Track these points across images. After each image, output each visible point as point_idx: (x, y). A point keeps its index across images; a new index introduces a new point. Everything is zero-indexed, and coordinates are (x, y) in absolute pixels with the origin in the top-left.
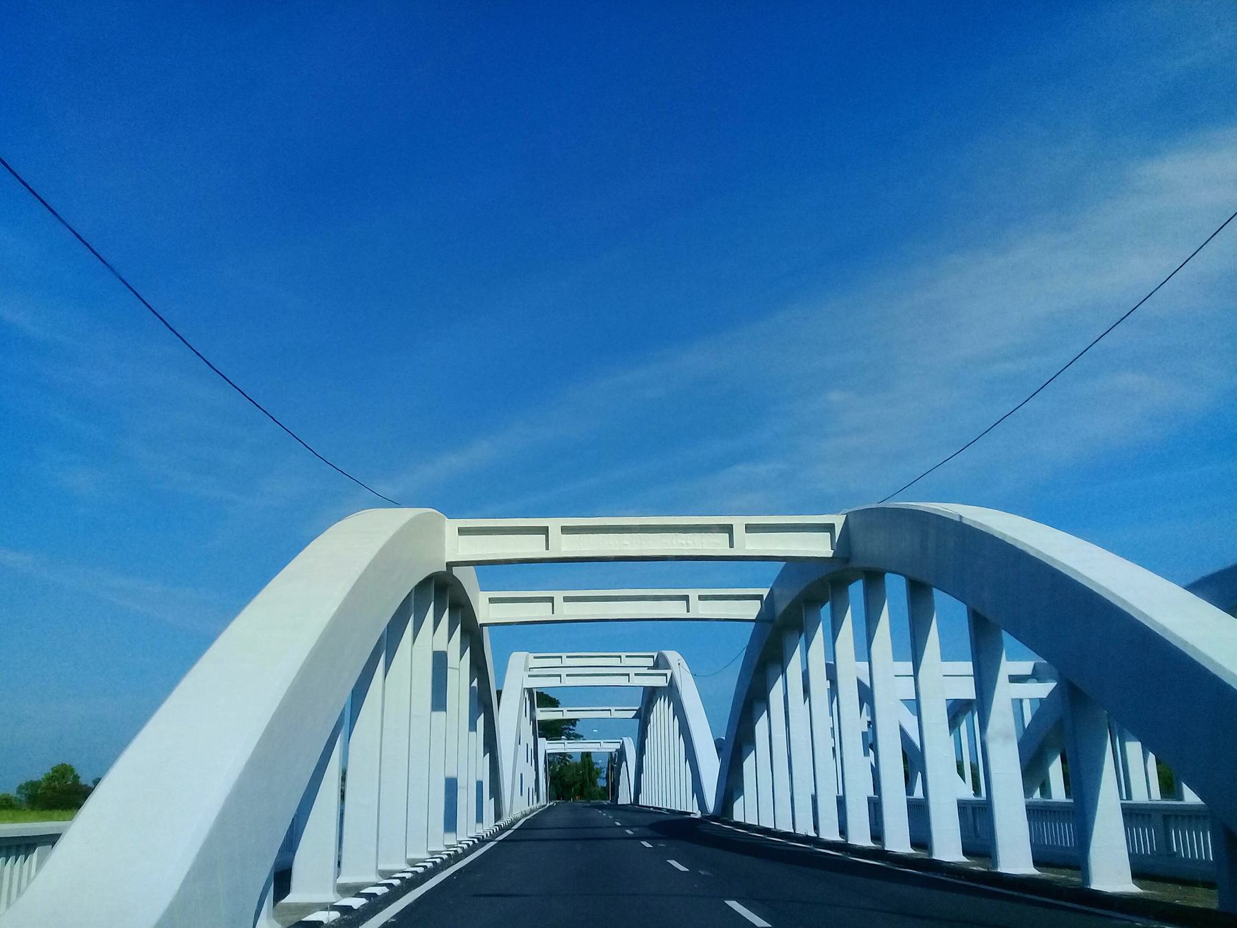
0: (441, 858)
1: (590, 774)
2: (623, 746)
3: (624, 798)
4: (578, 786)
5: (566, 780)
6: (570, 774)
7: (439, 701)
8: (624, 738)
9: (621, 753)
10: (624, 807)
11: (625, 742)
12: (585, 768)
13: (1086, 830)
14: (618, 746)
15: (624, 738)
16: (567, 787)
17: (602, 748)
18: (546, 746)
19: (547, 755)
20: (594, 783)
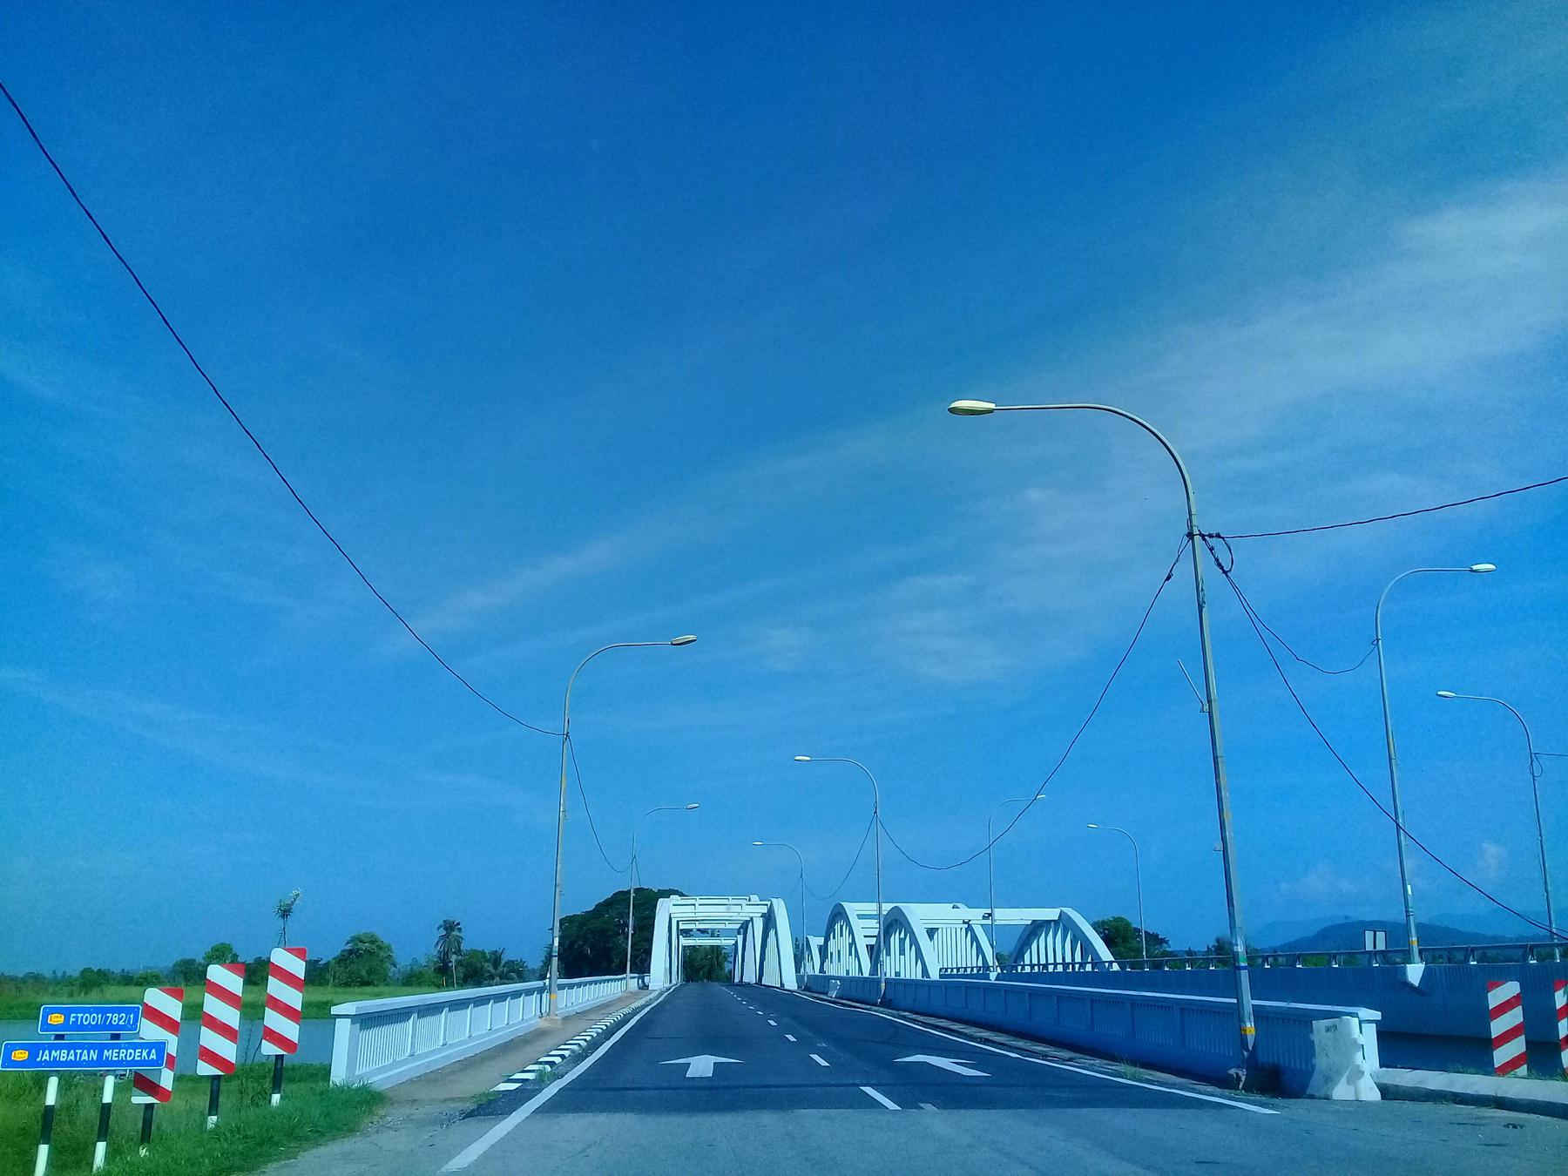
0: (606, 1025)
1: (717, 958)
2: (771, 909)
3: (737, 980)
4: (706, 969)
5: (696, 964)
6: (699, 958)
7: (1202, 578)
8: (773, 900)
9: (736, 944)
10: (737, 985)
11: (774, 903)
12: (713, 952)
13: (1530, 1104)
14: (734, 942)
15: (773, 900)
16: (697, 970)
17: (726, 942)
18: (684, 942)
19: (684, 947)
20: (721, 967)
